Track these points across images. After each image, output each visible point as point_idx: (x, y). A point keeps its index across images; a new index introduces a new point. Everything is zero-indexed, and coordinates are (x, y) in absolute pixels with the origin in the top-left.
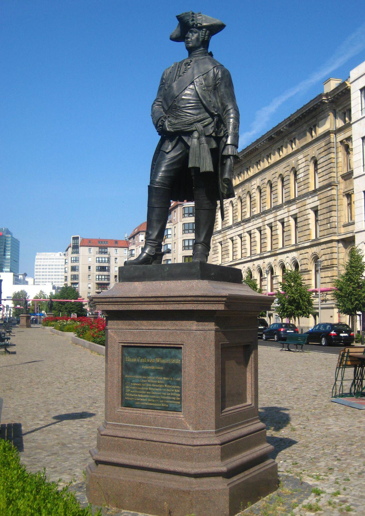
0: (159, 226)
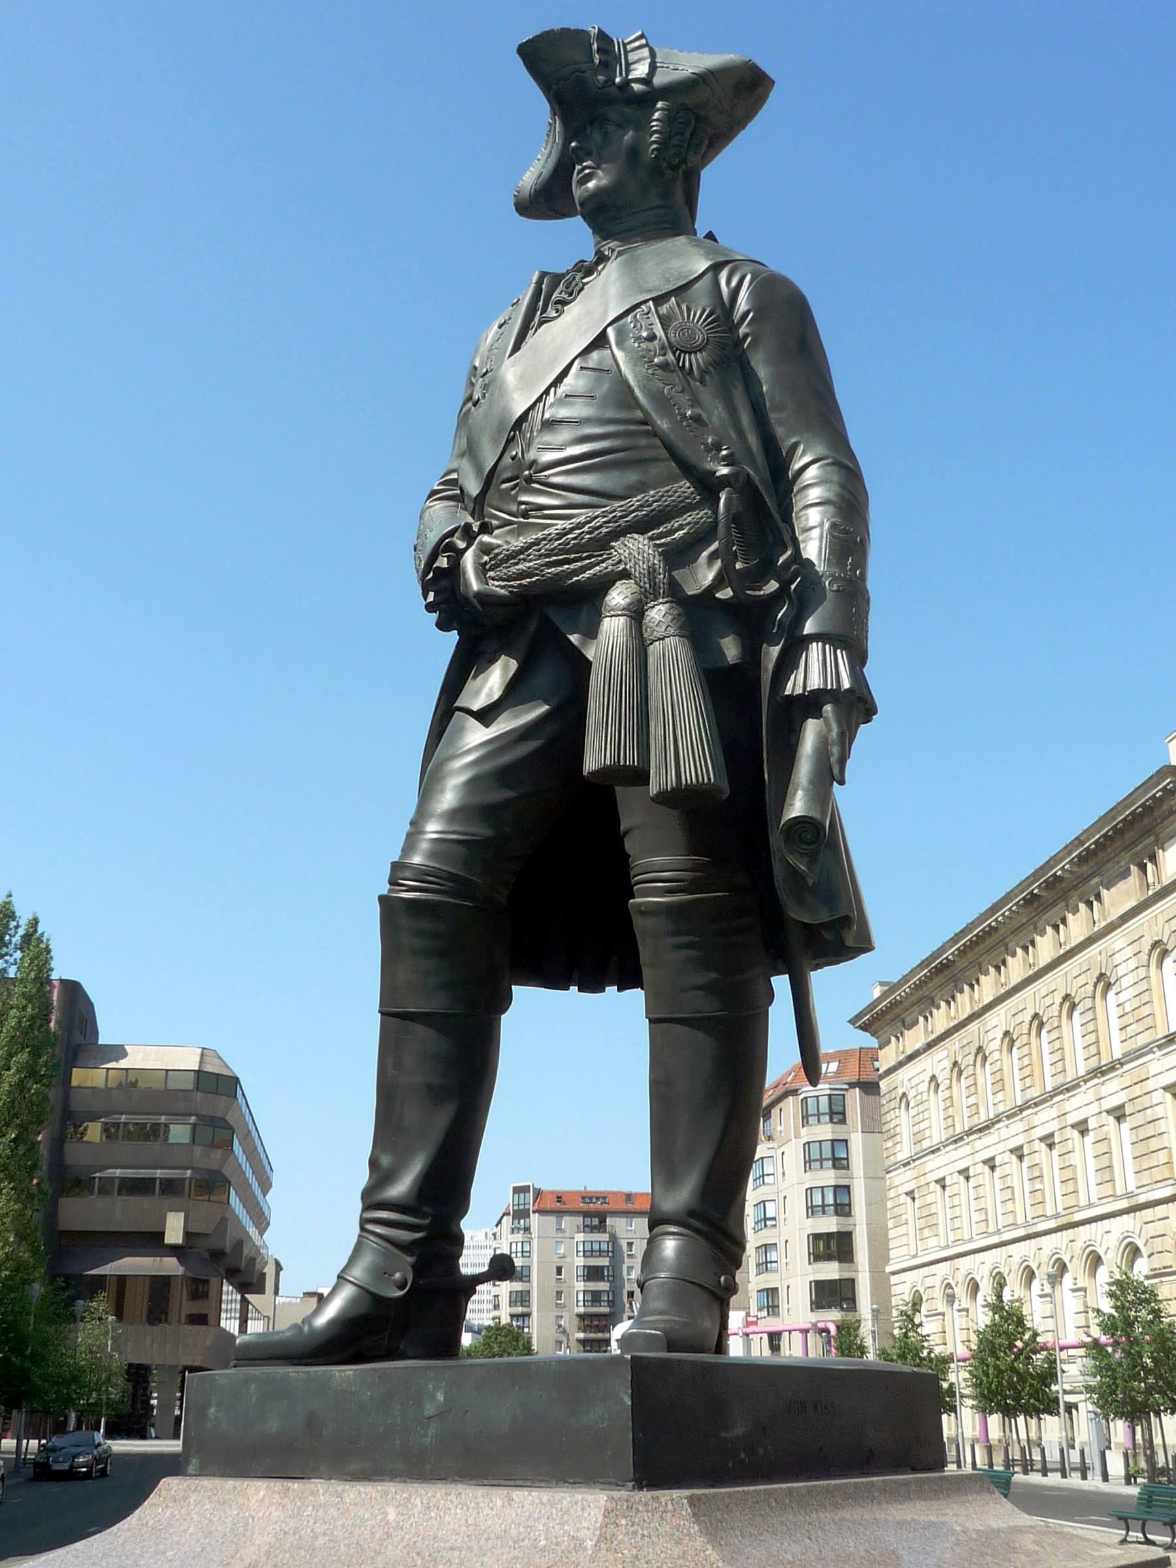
0: (443, 1117)
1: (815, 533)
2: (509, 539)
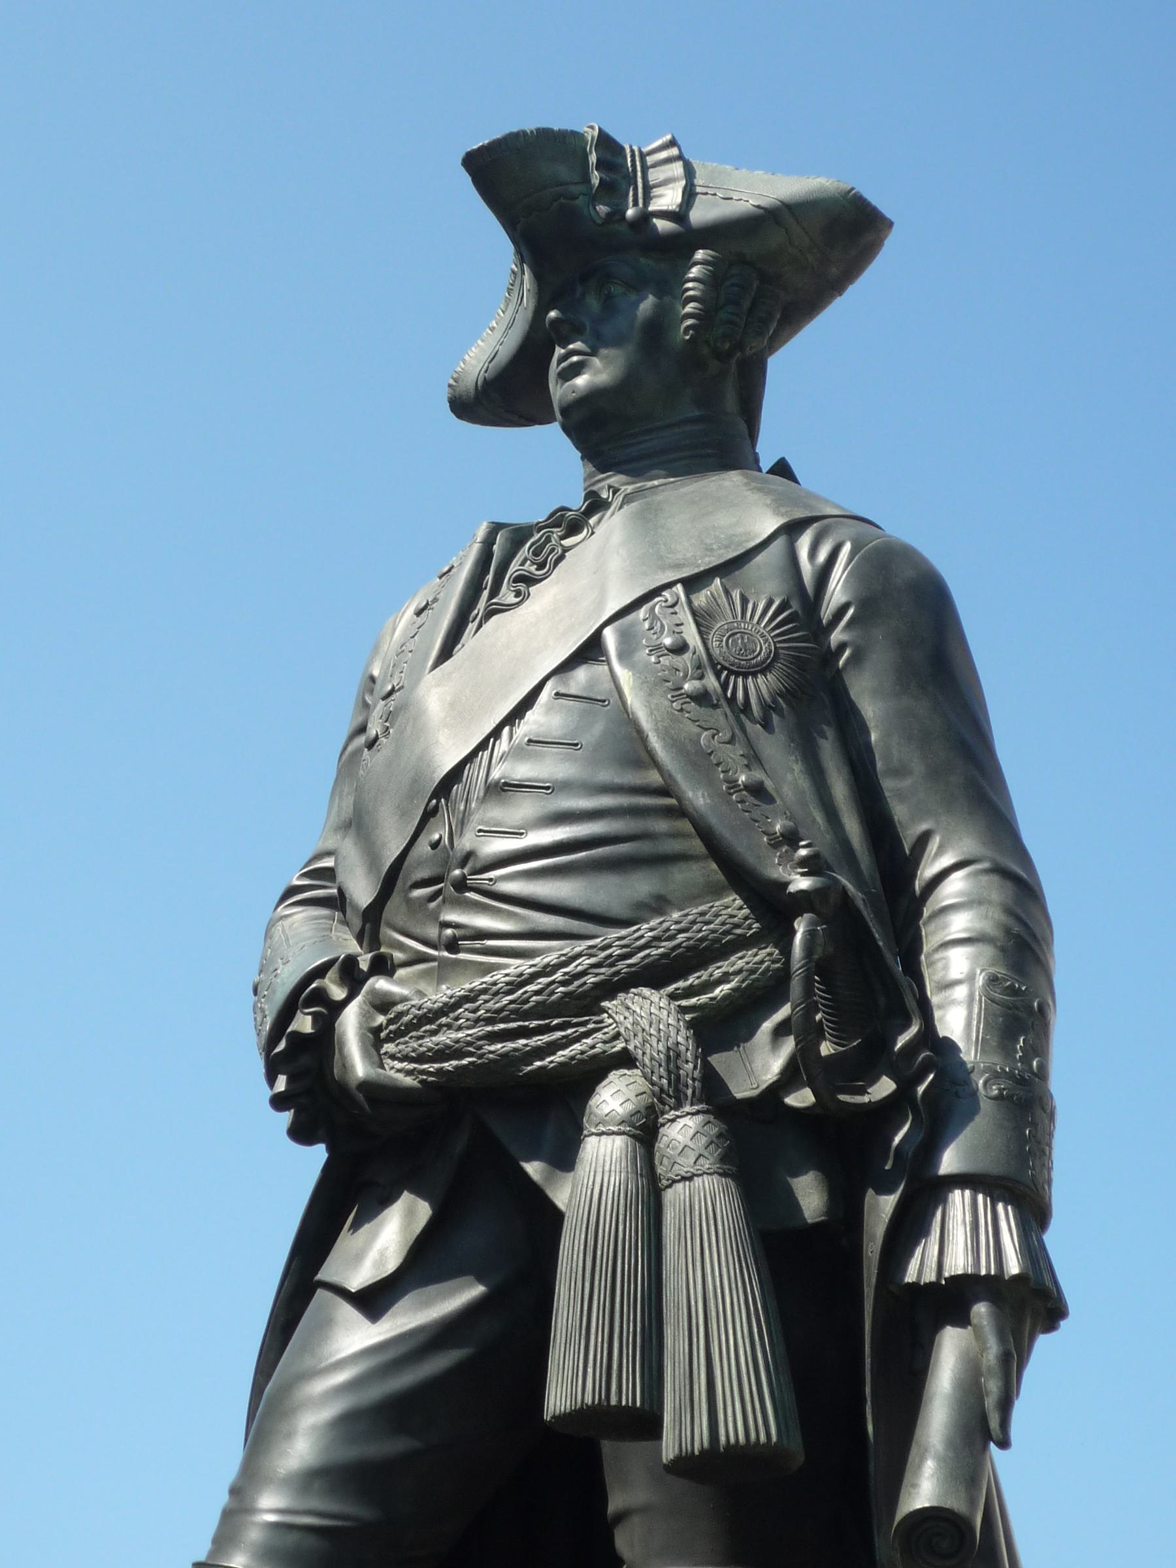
1: (961, 992)
2: (422, 986)
